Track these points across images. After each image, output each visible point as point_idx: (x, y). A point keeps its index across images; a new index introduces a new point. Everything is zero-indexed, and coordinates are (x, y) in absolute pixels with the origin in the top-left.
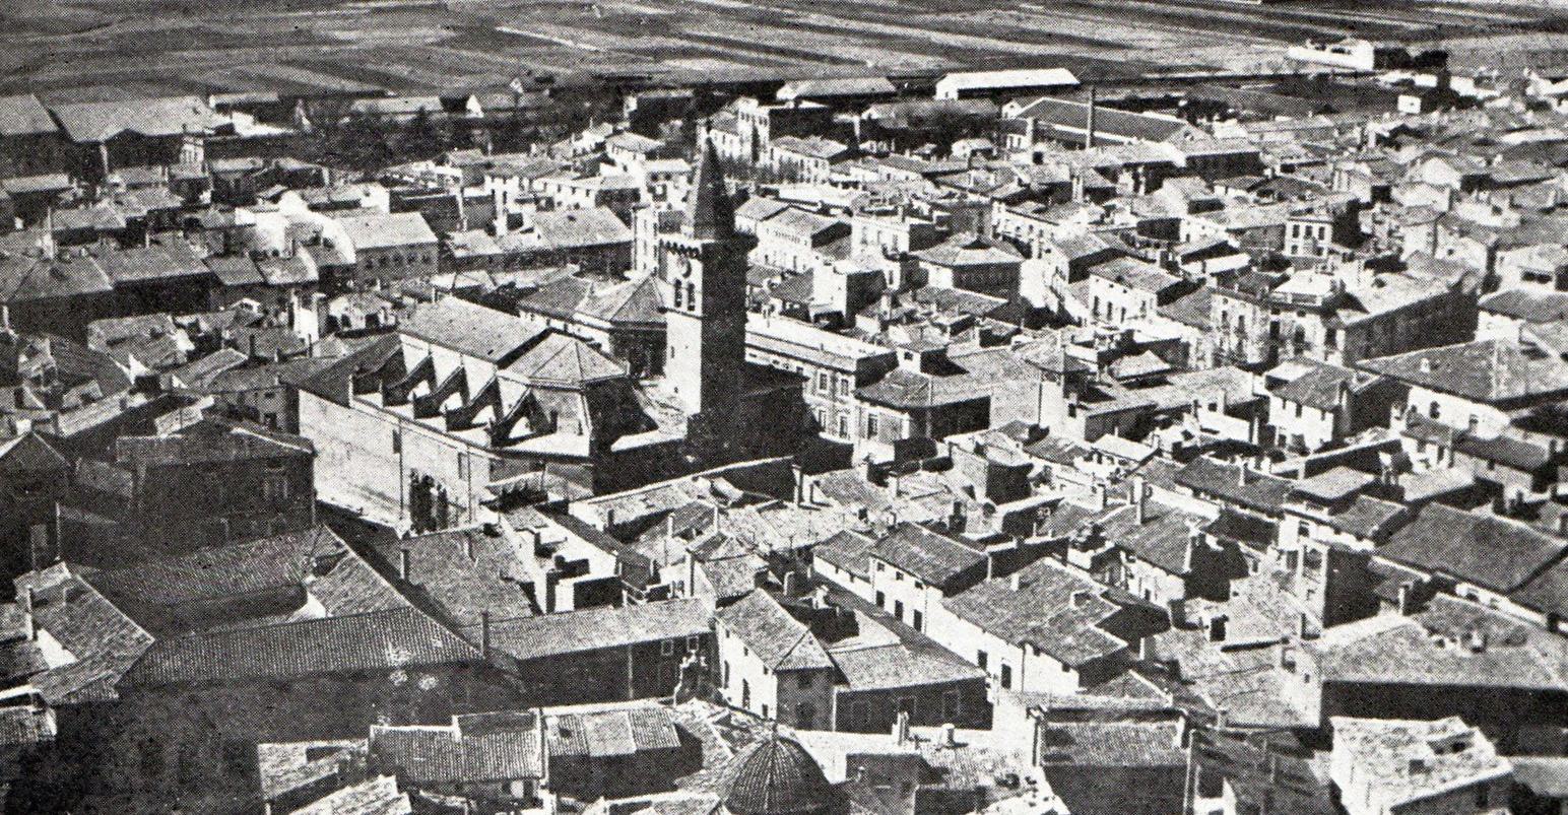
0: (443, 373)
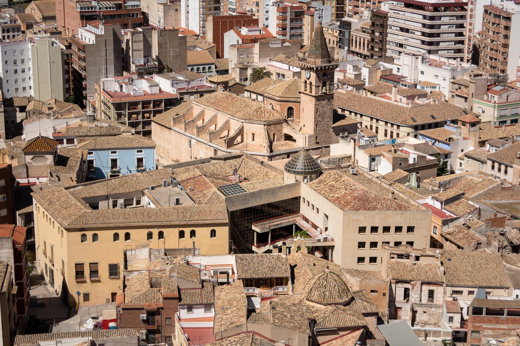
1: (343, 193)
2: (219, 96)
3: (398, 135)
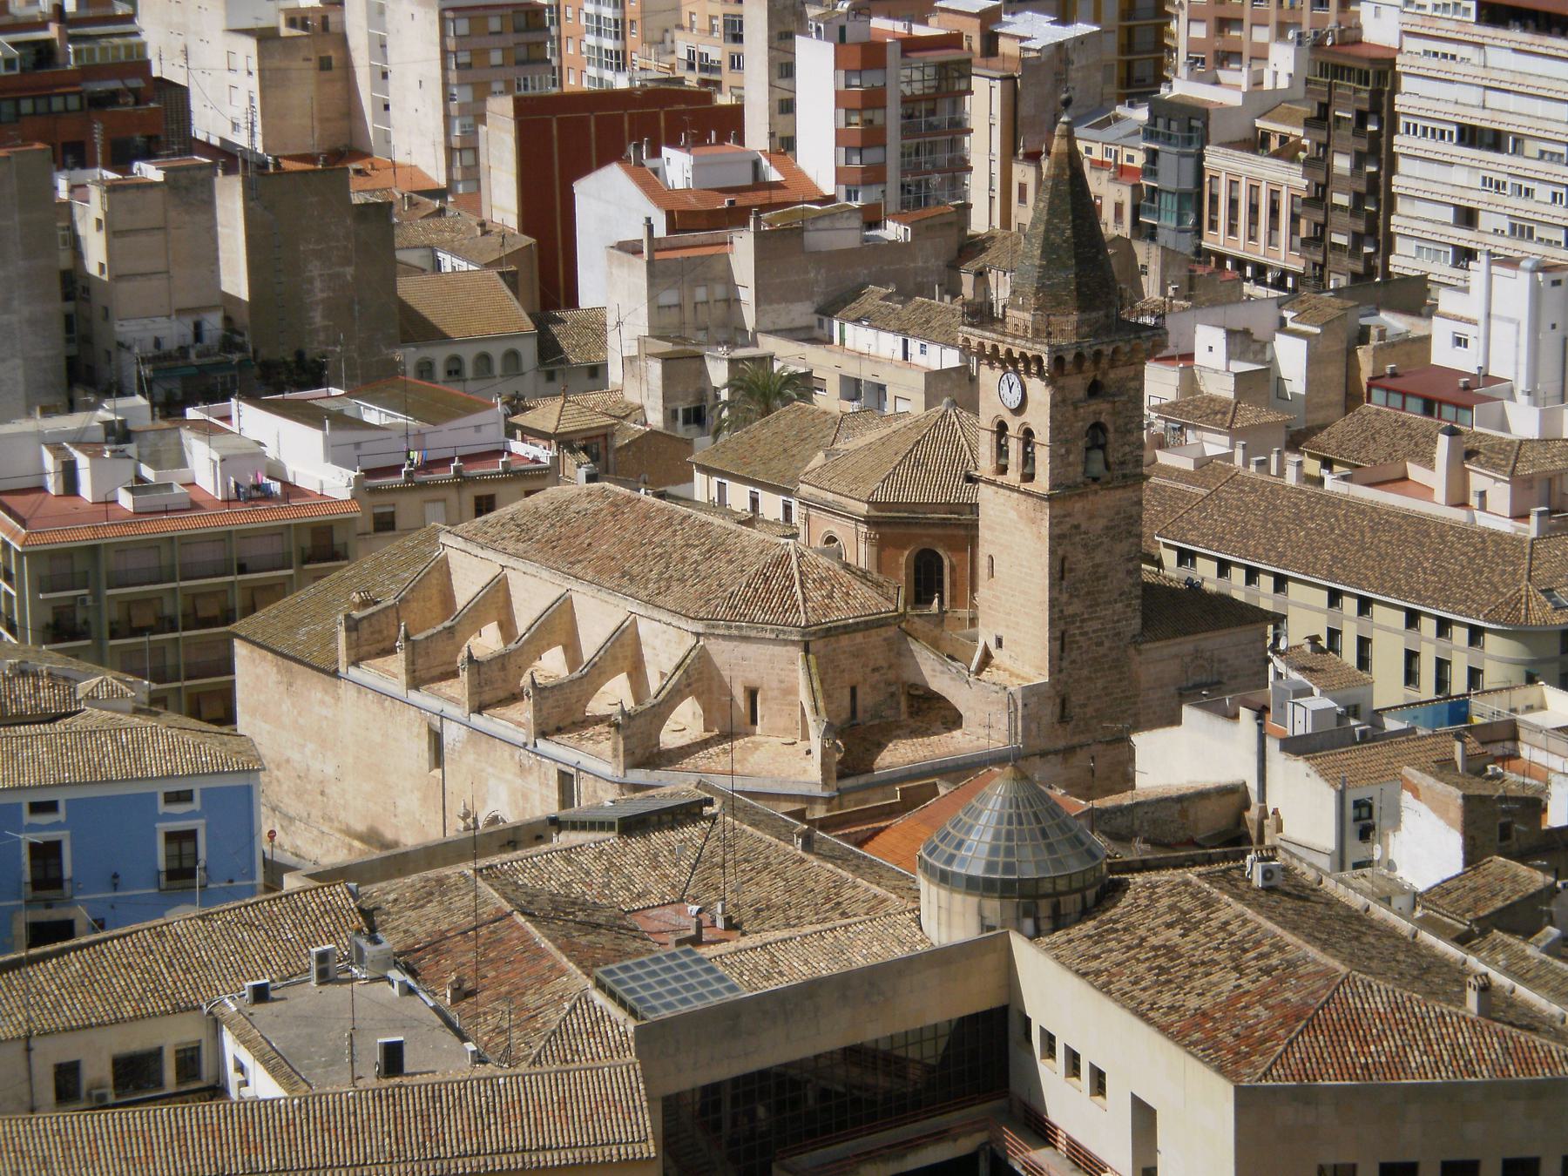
0: (594, 630)
1: (1227, 987)
2: (574, 507)
3: (1474, 675)
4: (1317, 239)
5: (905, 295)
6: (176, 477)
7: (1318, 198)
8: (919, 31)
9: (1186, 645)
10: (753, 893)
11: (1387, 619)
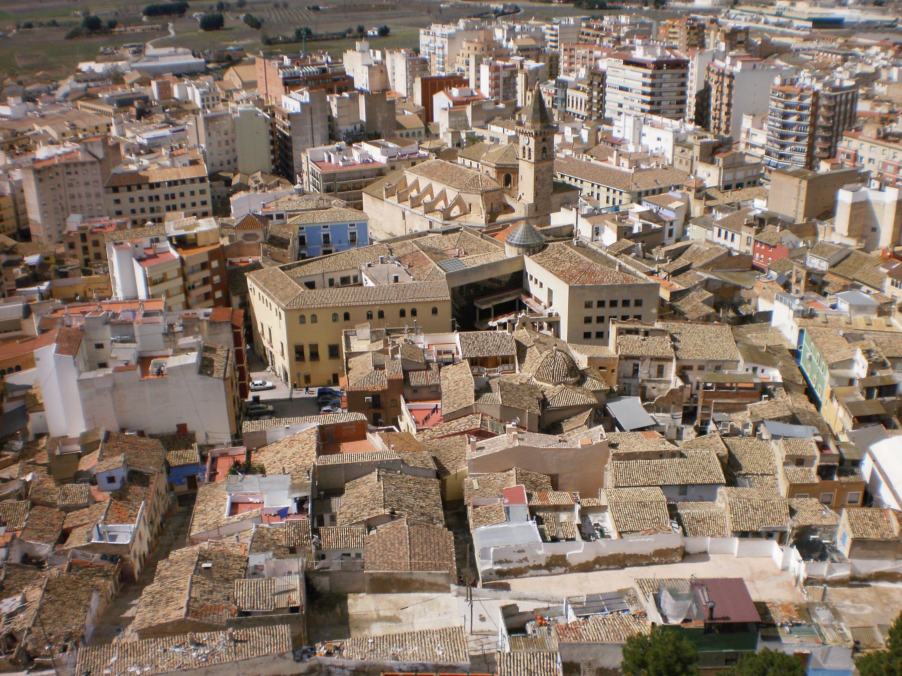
3: (620, 201)
4: (590, 109)
5: (504, 119)
6: (351, 158)
7: (590, 101)
8: (507, 64)
9: (562, 195)
10: (470, 247)
11: (603, 190)
